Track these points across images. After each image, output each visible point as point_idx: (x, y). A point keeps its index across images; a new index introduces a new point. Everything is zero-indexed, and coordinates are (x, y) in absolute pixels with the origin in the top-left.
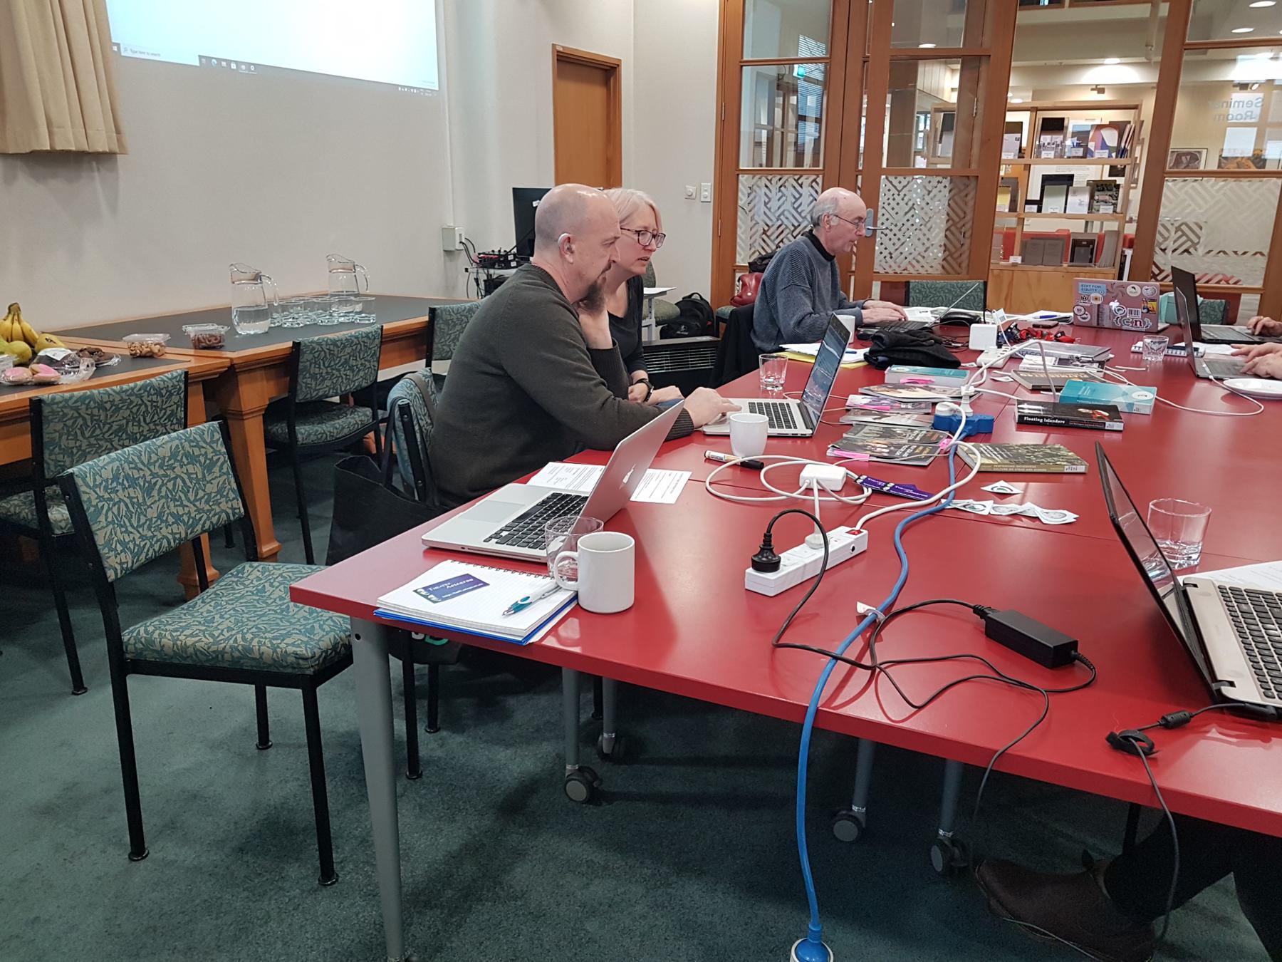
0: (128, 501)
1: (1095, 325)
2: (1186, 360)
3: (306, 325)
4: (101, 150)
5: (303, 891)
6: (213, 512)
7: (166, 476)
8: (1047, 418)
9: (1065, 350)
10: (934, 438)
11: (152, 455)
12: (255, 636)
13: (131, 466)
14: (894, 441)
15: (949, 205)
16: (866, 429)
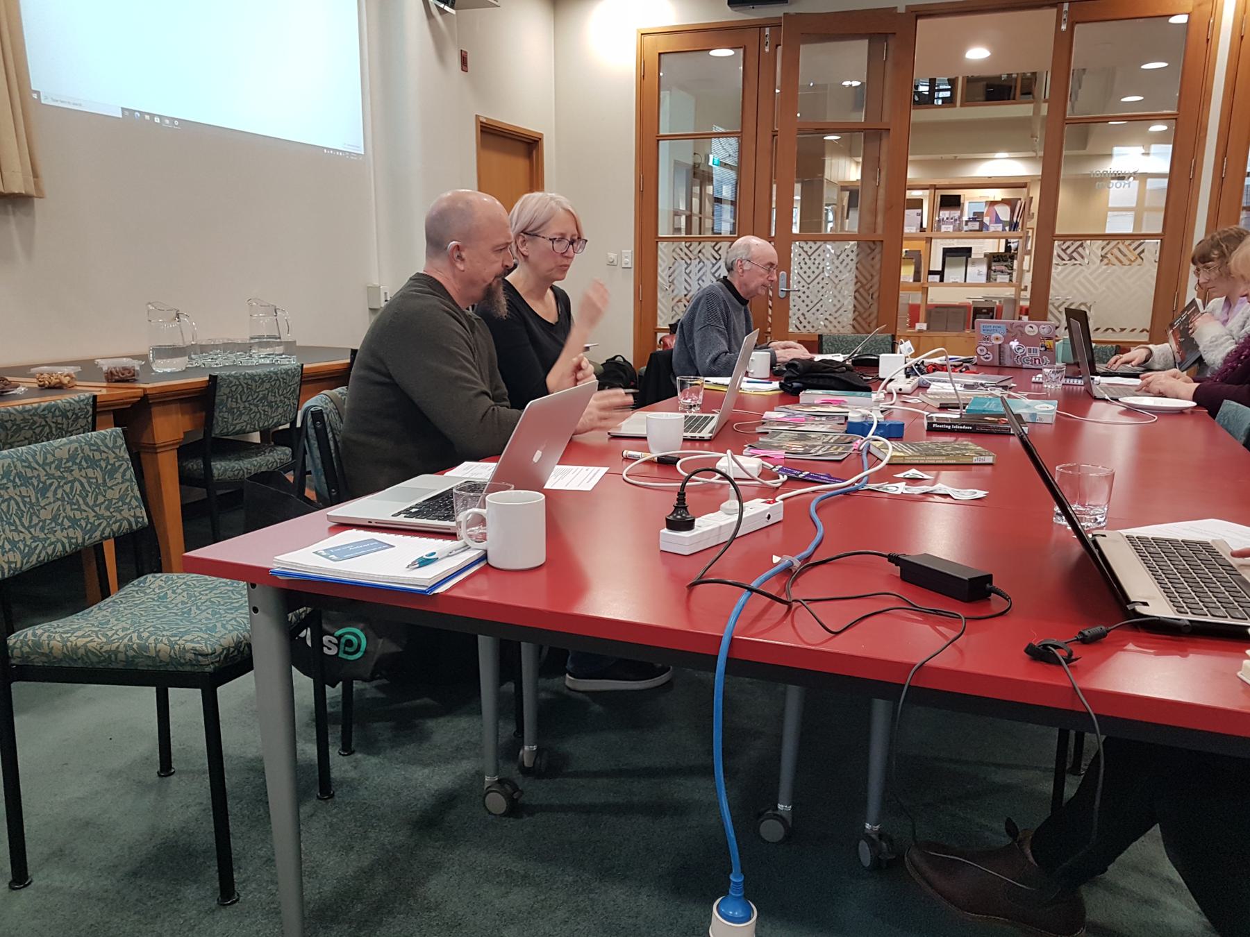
0: (19, 499)
1: (997, 364)
2: (1083, 388)
3: (225, 366)
4: (16, 192)
5: (200, 912)
6: (113, 519)
7: (63, 478)
8: (955, 425)
9: (969, 379)
10: (848, 440)
11: (49, 456)
12: (152, 635)
13: (24, 464)
14: (809, 443)
15: (857, 268)
16: (782, 435)
